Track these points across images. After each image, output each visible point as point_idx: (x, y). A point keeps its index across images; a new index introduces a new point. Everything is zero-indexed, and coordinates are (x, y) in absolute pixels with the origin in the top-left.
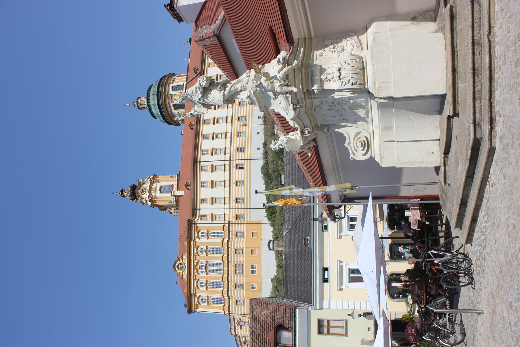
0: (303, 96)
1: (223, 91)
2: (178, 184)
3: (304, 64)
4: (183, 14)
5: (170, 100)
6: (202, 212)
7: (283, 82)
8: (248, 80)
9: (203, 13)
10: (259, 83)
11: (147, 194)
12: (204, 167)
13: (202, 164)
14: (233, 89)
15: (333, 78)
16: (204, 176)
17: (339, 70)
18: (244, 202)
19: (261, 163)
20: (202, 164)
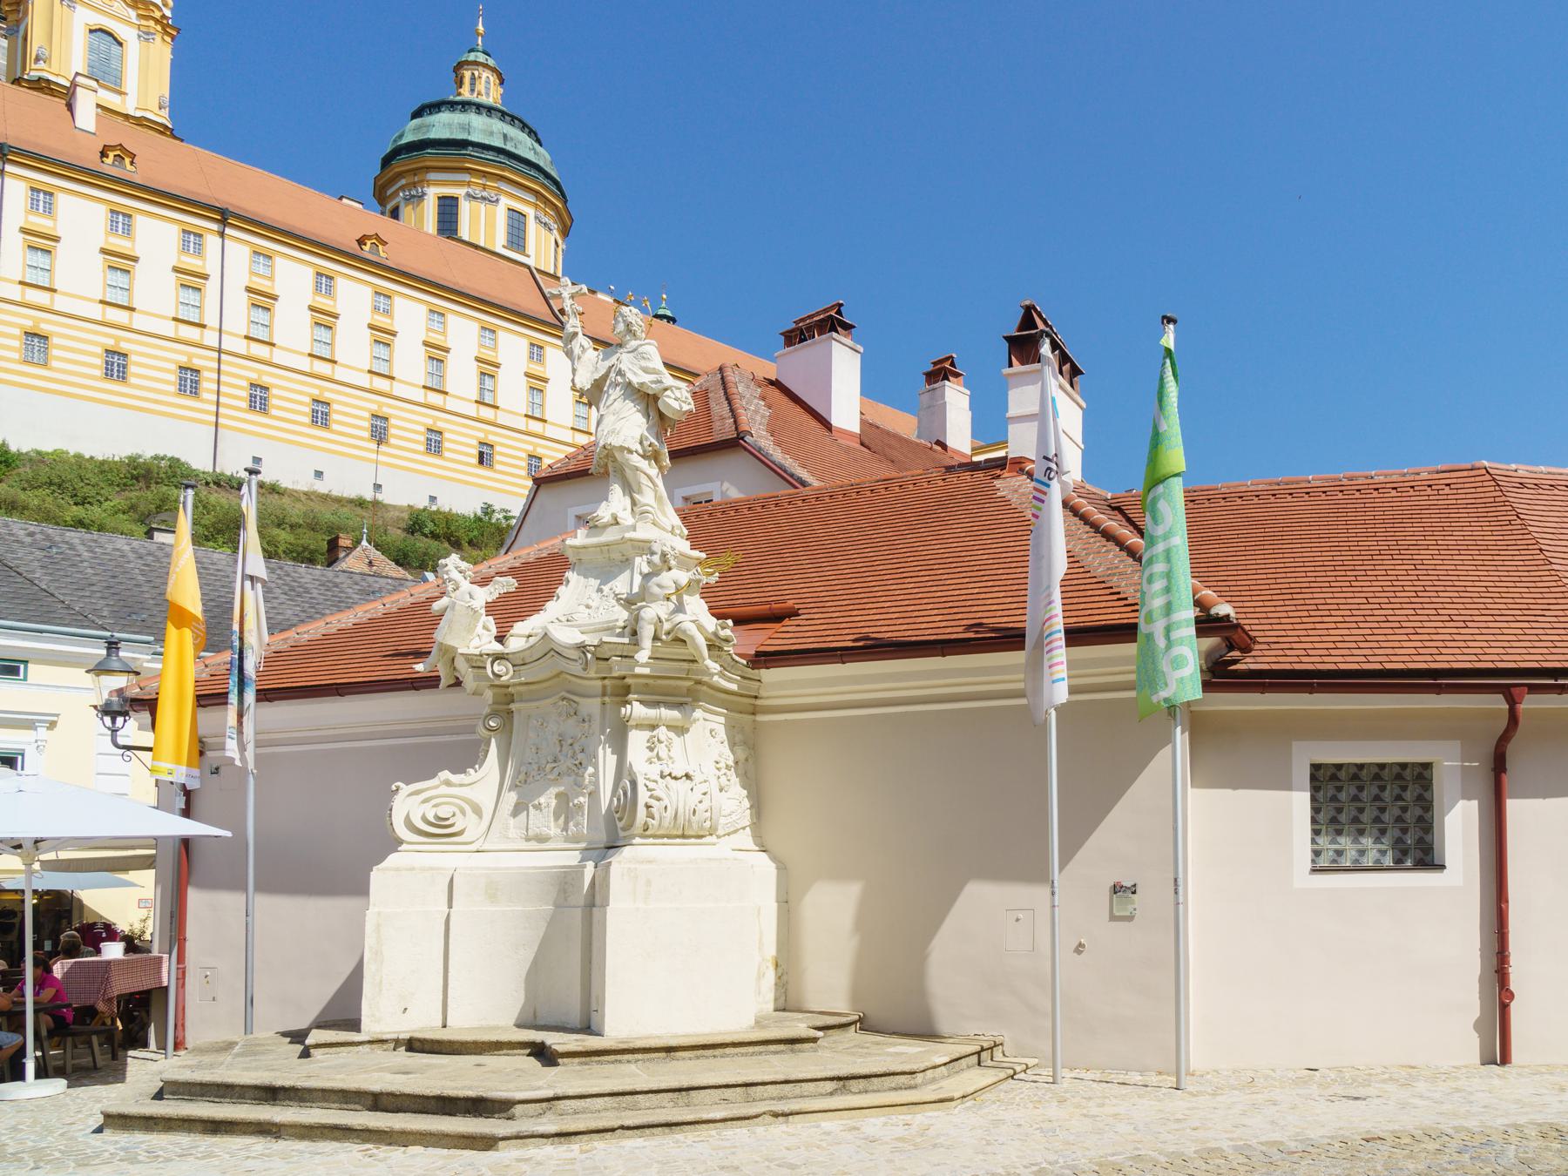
2: (127, 117)
5: (478, 192)
7: (667, 626)
9: (799, 409)
10: (673, 563)
13: (212, 242)
15: (659, 758)
16: (157, 235)
17: (688, 776)
18: (26, 362)
19: (199, 460)
20: (212, 242)
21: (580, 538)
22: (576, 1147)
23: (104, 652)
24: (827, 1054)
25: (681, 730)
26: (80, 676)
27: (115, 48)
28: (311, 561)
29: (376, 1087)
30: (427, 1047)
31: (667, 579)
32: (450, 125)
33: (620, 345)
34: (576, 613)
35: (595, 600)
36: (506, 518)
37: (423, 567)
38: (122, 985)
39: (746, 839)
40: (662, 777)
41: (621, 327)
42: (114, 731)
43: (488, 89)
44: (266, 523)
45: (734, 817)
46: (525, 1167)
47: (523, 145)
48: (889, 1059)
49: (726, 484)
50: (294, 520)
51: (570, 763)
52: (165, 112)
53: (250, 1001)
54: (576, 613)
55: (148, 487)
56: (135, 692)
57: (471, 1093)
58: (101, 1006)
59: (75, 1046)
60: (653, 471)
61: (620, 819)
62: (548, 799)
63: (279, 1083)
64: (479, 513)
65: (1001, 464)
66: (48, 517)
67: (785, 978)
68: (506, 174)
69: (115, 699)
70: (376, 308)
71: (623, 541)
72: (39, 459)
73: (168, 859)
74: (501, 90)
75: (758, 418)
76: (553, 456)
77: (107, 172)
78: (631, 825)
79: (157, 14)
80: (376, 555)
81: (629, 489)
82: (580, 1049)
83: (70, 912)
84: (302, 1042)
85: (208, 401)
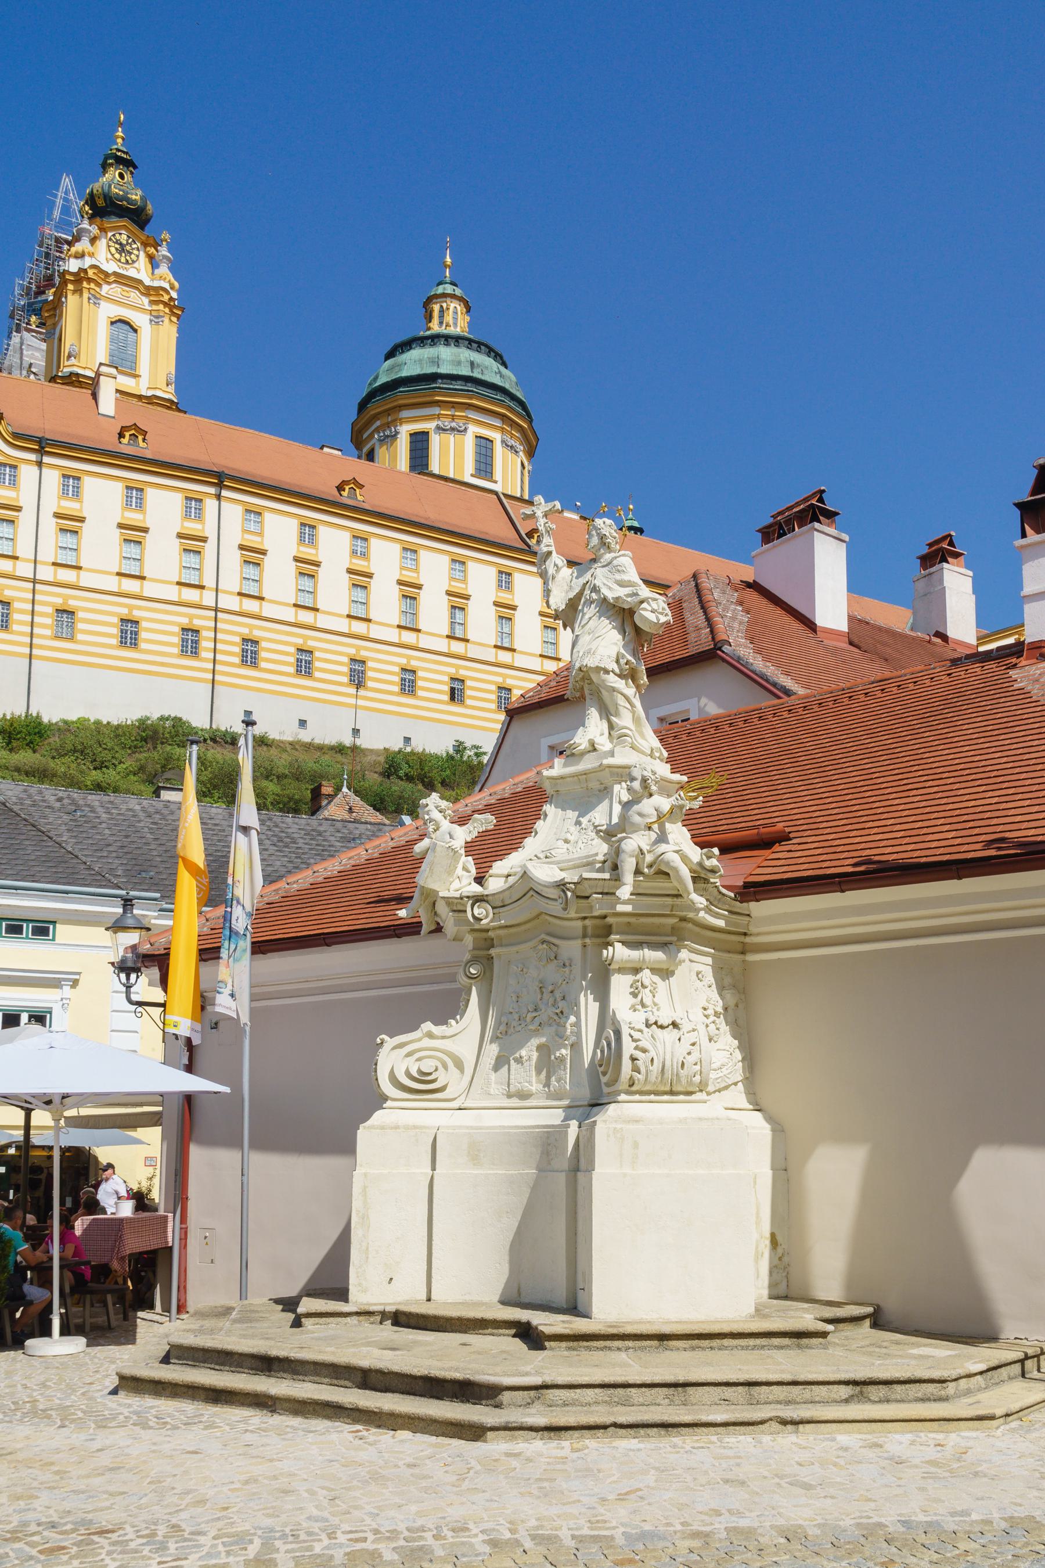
0: (596, 913)
1: (617, 671)
2: (140, 397)
3: (684, 924)
4: (784, 548)
5: (447, 423)
6: (28, 473)
7: (649, 858)
8: (643, 753)
9: (779, 611)
10: (654, 788)
11: (111, 267)
12: (200, 511)
13: (211, 504)
14: (621, 701)
15: (643, 1005)
16: (164, 504)
17: (675, 1025)
19: (199, 720)
20: (211, 504)
21: (558, 768)
22: (566, 1444)
23: (120, 910)
24: (839, 1352)
25: (665, 973)
26: (100, 935)
27: (132, 335)
28: (296, 811)
29: (365, 1363)
30: (413, 1322)
31: (648, 806)
32: (420, 360)
33: (594, 561)
34: (556, 849)
35: (574, 833)
36: (477, 755)
37: (398, 811)
38: (133, 1244)
39: (738, 1096)
40: (648, 1025)
41: (595, 541)
42: (128, 987)
43: (455, 319)
44: (263, 773)
45: (725, 1071)
46: (514, 1463)
47: (490, 370)
48: (913, 1362)
49: (705, 700)
50: (281, 770)
51: (551, 1011)
52: (171, 389)
53: (244, 1265)
54: (556, 849)
55: (155, 748)
56: (146, 948)
57: (458, 1376)
58: (115, 1265)
59: (92, 1306)
60: (631, 691)
61: (604, 1074)
62: (529, 1051)
63: (274, 1353)
64: (451, 751)
65: (1017, 650)
66: (73, 783)
67: (786, 1259)
68: (474, 402)
69: (130, 955)
70: (354, 552)
71: (602, 768)
72: (66, 728)
73: (173, 1117)
74: (468, 318)
75: (736, 625)
76: (522, 686)
77: (125, 453)
78: (615, 1080)
79: (166, 298)
80: (356, 800)
81: (607, 712)
82: (567, 1331)
83: (86, 1169)
84: (294, 1311)
85: (206, 660)
